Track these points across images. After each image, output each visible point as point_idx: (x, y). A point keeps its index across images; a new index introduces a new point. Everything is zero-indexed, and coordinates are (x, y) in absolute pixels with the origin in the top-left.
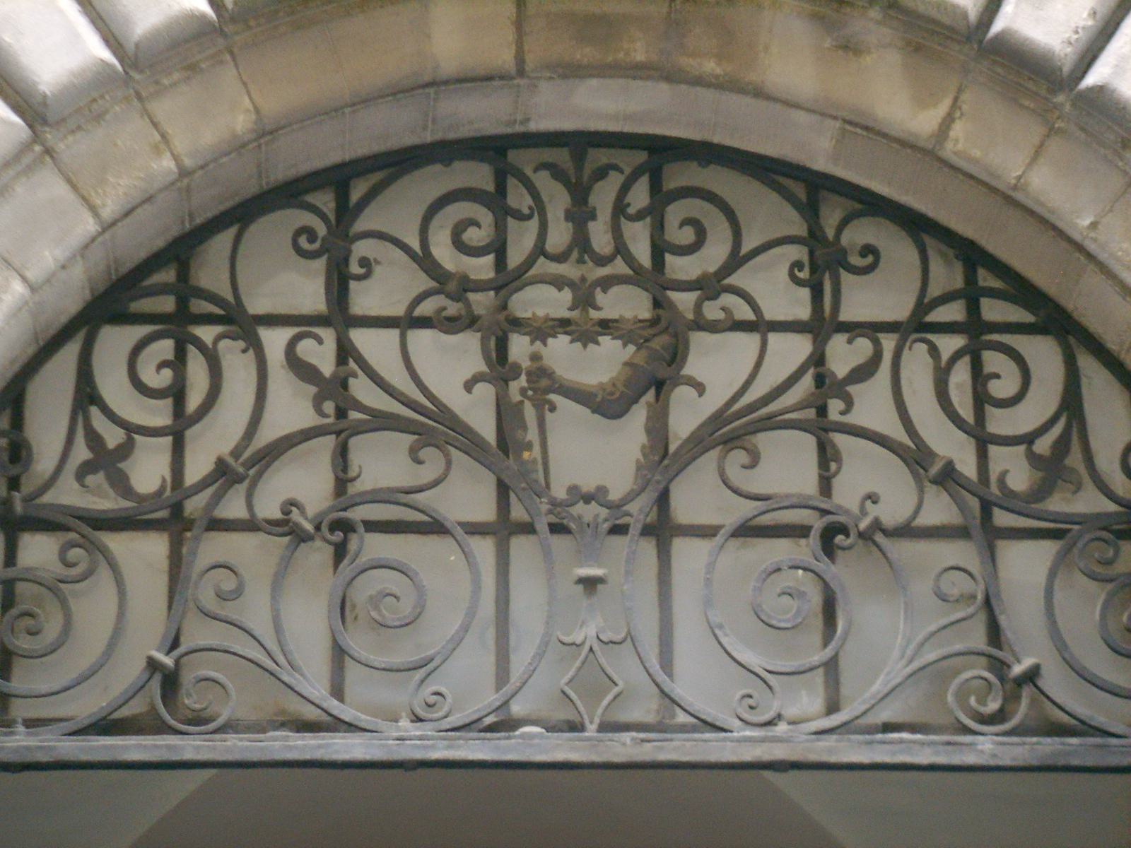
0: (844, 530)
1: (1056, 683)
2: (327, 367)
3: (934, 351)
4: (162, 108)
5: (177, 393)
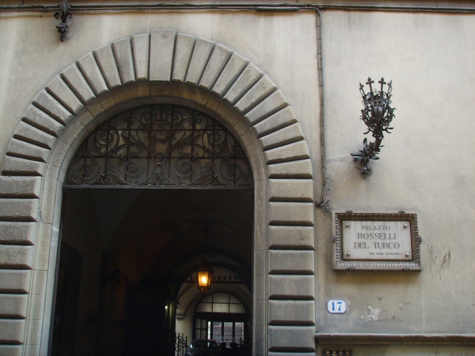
0: (193, 158)
1: (220, 180)
2: (126, 136)
3: (207, 133)
4: (102, 103)
5: (107, 139)
